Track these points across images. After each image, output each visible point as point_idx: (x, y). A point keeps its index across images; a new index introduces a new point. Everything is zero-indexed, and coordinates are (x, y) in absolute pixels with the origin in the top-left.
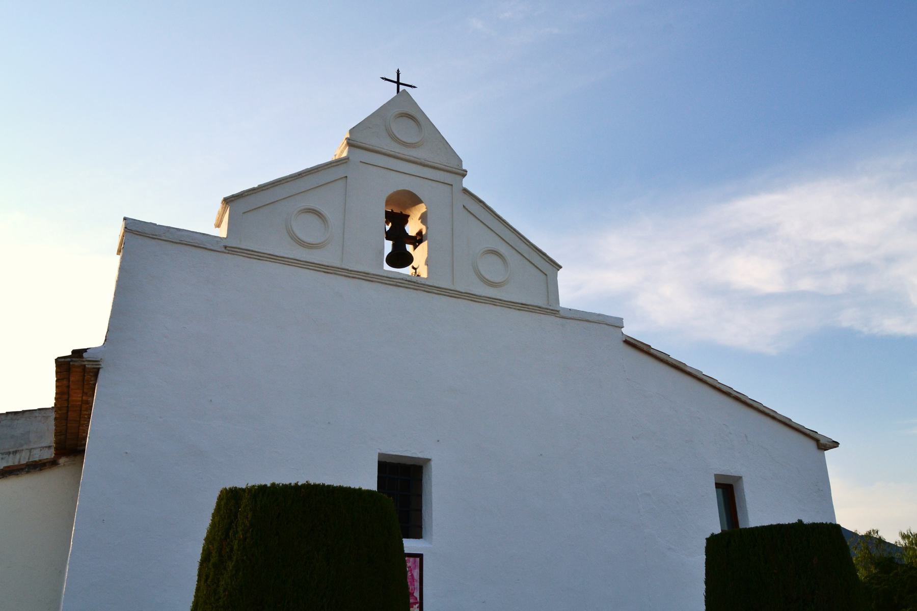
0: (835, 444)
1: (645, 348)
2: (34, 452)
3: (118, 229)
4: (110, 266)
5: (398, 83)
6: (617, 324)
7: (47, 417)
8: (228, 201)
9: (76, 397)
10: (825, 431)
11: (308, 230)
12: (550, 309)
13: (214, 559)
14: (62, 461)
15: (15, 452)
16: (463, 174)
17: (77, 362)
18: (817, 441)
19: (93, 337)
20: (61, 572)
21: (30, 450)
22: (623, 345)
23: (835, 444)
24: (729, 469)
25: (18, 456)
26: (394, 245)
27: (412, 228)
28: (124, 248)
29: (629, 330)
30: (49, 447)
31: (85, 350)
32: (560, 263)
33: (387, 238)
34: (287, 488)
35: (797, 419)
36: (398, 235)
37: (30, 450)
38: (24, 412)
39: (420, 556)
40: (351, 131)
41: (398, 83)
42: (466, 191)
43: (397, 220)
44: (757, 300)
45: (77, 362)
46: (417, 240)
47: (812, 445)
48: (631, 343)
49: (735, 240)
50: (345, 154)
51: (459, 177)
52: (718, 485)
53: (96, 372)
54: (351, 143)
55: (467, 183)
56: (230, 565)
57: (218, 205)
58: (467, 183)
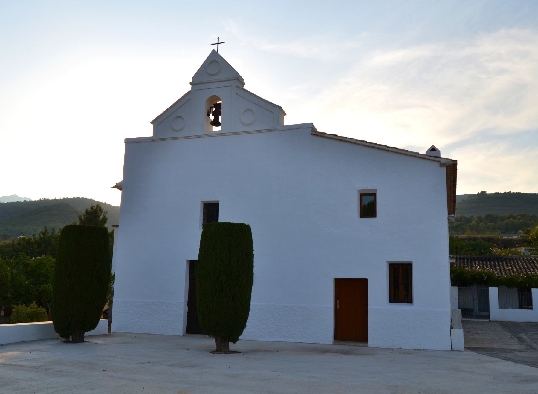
1: (396, 150)
18: (440, 162)
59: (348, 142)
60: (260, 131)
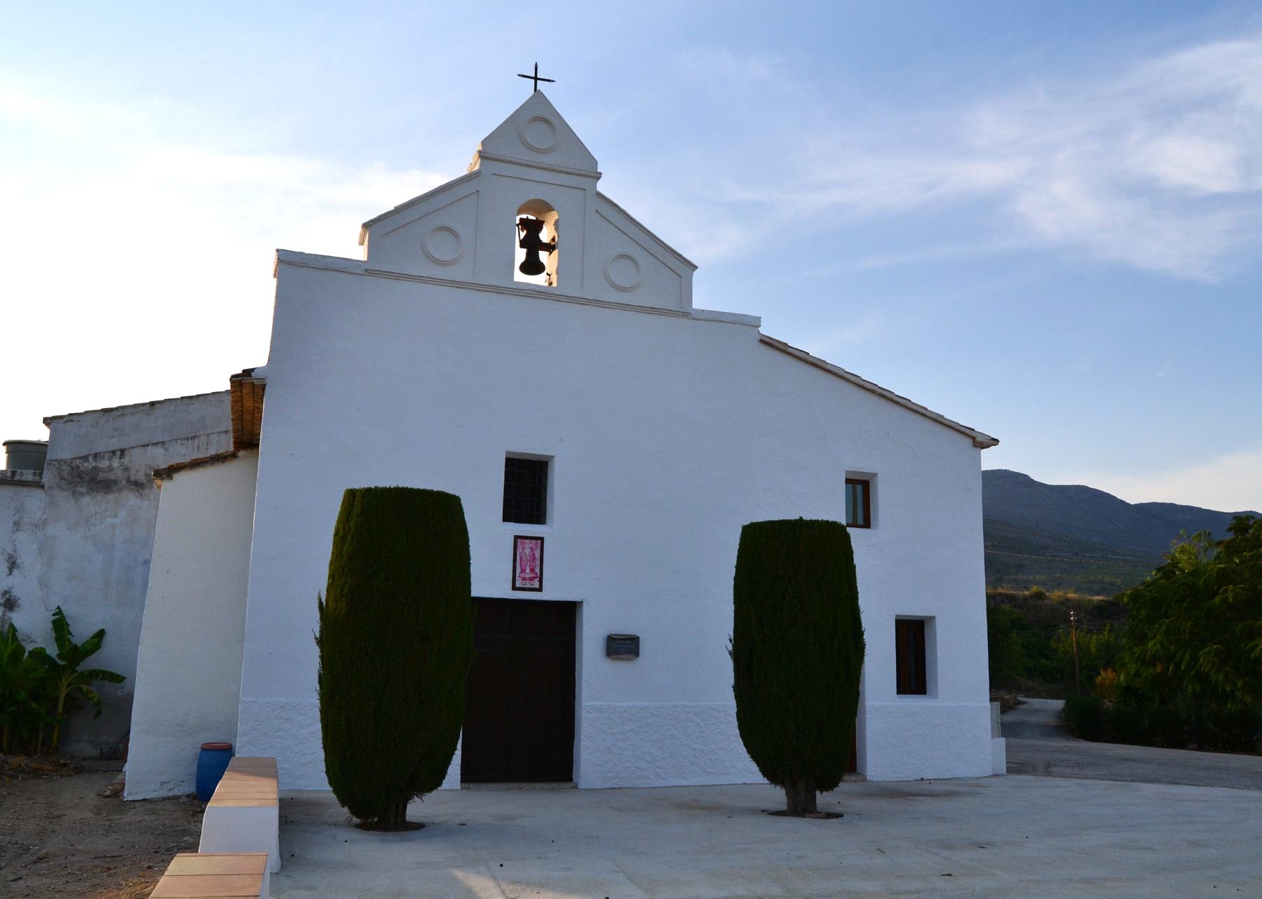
0: (995, 442)
1: (782, 347)
2: (212, 437)
3: (272, 259)
4: (269, 286)
5: (536, 79)
6: (754, 323)
7: (221, 402)
8: (366, 226)
9: (249, 404)
10: (982, 427)
11: (442, 247)
12: (684, 313)
13: (341, 534)
14: (241, 453)
15: (194, 437)
16: (598, 176)
17: (246, 380)
18: (974, 438)
19: (256, 356)
20: (247, 551)
21: (208, 435)
22: (757, 343)
23: (995, 442)
24: (861, 465)
25: (196, 441)
26: (528, 254)
27: (545, 236)
28: (278, 274)
29: (765, 330)
30: (226, 432)
31: (253, 370)
32: (696, 263)
33: (522, 246)
34: (384, 489)
35: (950, 415)
36: (532, 244)
37: (208, 435)
38: (198, 396)
39: (542, 539)
40: (484, 142)
41: (536, 79)
42: (599, 195)
43: (532, 228)
44: (1191, 204)
45: (246, 380)
46: (550, 248)
47: (968, 442)
48: (768, 343)
49: (1169, 113)
50: (477, 168)
51: (592, 181)
52: (848, 481)
53: (263, 387)
54: (482, 155)
55: (601, 187)
56: (349, 537)
57: (359, 229)
58: (601, 187)
59: (923, 415)
60: (653, 310)
